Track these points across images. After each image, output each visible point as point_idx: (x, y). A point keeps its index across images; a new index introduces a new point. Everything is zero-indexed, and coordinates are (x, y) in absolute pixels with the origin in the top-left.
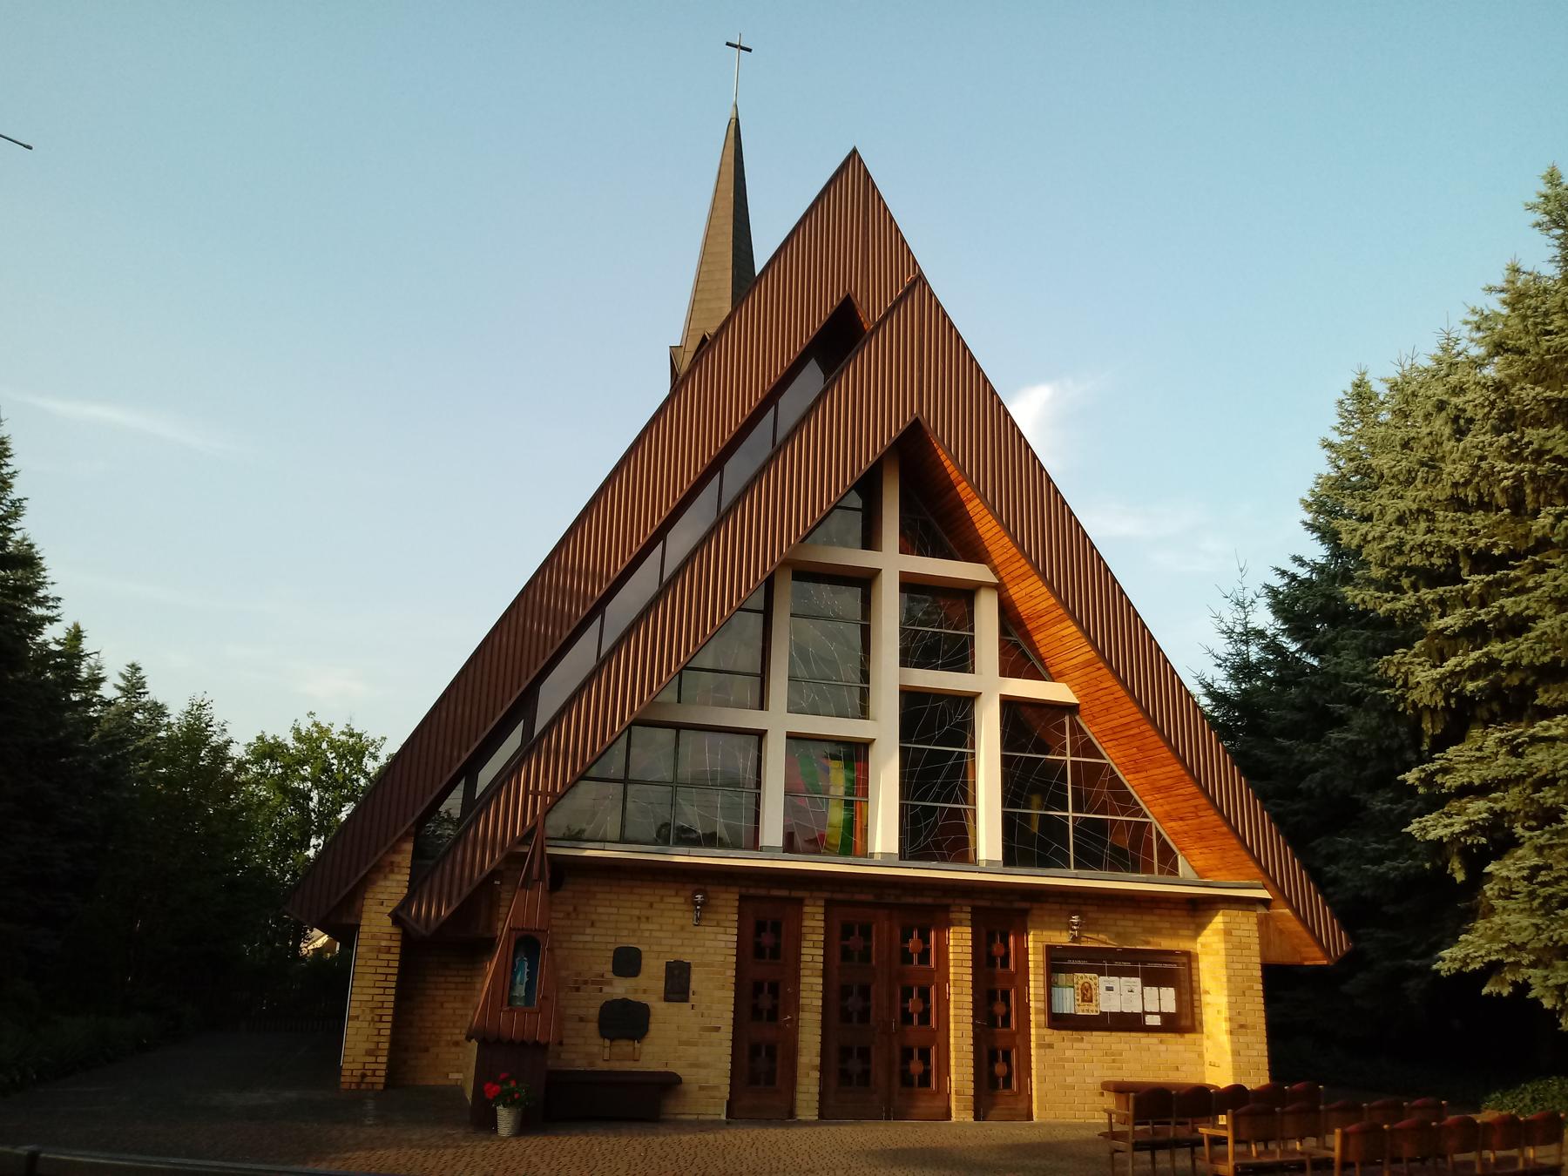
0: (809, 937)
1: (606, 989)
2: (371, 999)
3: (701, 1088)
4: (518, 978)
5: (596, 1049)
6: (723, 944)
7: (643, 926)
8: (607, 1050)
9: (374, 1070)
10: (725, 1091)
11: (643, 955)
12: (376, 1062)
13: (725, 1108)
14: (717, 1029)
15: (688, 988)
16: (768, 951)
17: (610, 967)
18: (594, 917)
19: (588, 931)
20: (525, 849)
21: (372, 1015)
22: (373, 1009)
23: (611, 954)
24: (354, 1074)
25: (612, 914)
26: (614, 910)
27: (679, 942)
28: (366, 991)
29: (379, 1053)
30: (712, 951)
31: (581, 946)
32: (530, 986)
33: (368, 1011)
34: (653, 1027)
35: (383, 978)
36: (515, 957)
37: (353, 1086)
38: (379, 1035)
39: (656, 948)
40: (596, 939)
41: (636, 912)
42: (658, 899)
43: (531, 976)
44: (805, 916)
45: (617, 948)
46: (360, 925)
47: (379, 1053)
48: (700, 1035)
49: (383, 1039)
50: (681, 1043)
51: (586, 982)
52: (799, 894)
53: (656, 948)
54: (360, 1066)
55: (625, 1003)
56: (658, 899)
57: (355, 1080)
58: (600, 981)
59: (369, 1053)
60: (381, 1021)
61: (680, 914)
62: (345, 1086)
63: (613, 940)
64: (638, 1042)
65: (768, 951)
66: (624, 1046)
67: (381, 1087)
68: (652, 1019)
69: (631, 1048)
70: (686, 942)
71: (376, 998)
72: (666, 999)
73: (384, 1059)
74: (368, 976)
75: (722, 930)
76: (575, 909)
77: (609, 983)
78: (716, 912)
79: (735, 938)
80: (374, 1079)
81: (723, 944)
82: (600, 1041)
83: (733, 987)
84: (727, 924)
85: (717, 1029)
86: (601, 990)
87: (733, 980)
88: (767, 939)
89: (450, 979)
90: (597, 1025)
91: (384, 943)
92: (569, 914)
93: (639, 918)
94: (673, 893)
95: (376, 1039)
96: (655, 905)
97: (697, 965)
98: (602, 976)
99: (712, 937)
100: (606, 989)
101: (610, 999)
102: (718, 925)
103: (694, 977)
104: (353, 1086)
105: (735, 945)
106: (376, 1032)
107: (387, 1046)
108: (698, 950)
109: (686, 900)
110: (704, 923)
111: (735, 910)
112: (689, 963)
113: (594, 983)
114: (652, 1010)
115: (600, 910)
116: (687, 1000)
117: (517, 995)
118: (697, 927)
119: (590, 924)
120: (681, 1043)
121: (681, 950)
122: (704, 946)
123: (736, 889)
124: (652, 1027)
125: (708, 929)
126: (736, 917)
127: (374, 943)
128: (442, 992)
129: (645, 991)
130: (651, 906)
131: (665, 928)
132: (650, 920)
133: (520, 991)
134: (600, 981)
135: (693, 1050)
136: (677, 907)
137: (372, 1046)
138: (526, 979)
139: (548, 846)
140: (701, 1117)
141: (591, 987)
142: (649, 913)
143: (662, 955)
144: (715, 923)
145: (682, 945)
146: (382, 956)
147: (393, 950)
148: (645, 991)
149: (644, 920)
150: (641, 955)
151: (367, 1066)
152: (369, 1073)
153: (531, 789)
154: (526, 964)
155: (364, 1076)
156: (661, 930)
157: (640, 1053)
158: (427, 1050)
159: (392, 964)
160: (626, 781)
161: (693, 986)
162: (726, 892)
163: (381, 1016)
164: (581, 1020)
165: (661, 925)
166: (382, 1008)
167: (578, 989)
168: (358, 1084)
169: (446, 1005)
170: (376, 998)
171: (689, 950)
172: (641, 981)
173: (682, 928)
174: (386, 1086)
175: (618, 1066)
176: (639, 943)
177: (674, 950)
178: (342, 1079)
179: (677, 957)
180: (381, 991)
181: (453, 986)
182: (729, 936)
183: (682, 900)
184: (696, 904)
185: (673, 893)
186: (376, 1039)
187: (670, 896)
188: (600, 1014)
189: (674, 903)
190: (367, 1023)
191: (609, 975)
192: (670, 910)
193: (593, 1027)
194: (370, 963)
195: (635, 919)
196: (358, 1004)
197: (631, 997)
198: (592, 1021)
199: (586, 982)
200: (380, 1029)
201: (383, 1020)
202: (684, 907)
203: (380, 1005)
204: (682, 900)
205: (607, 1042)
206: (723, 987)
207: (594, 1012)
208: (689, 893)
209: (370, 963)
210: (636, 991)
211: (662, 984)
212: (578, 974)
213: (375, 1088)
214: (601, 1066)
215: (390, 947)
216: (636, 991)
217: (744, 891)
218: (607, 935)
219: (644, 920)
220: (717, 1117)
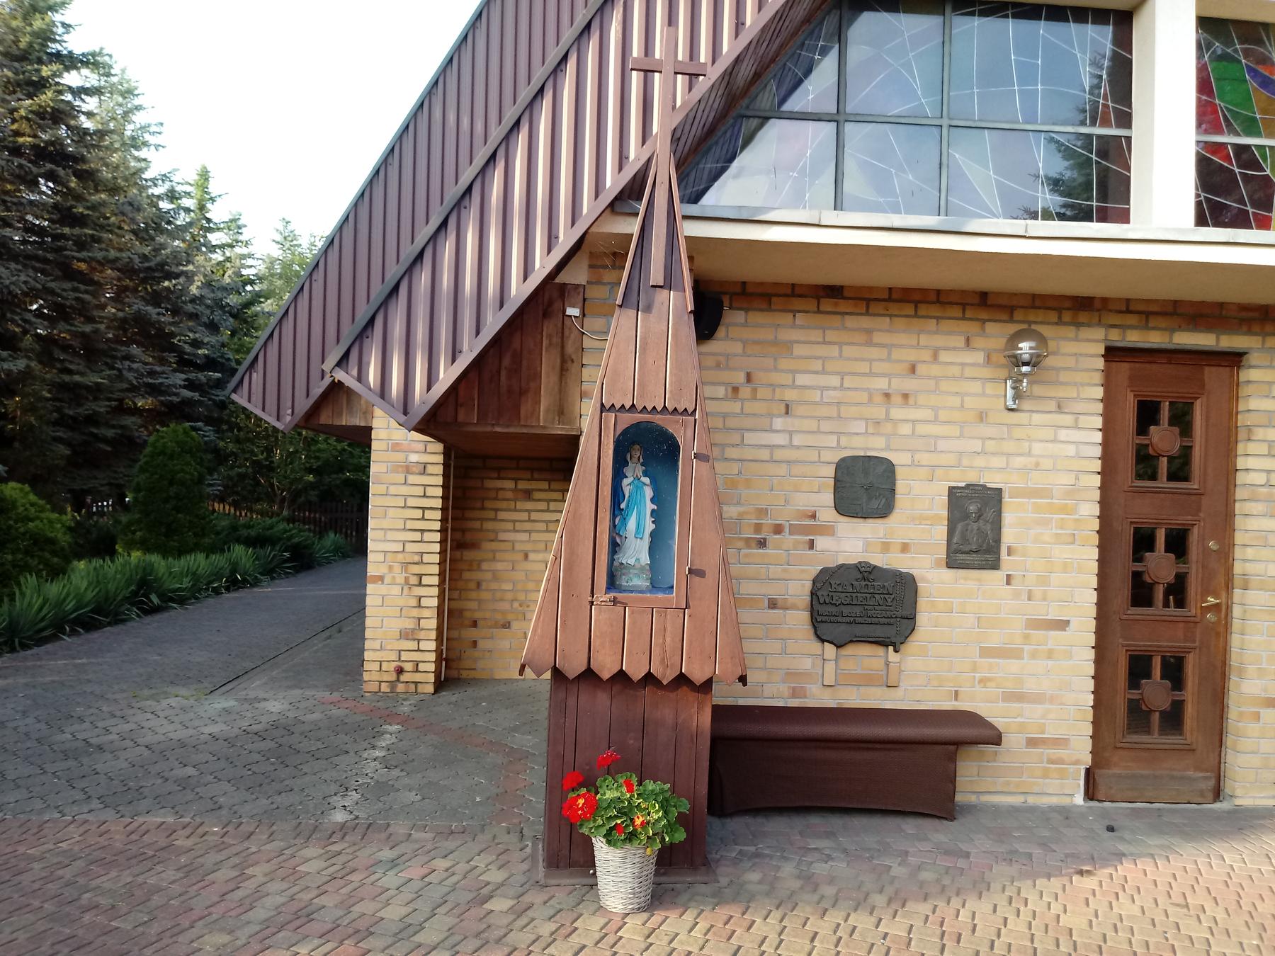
0: (1260, 433)
1: (822, 542)
2: (533, 514)
3: (1032, 743)
4: (632, 524)
5: (806, 664)
6: (1071, 450)
7: (897, 413)
8: (830, 667)
9: (417, 663)
10: (1082, 750)
11: (900, 473)
12: (419, 650)
13: (1082, 782)
14: (1063, 625)
15: (998, 541)
16: (1164, 462)
17: (828, 497)
18: (790, 395)
19: (779, 423)
20: (632, 227)
21: (404, 575)
22: (405, 565)
23: (830, 471)
24: (384, 668)
25: (828, 388)
26: (834, 381)
27: (976, 445)
28: (391, 536)
29: (422, 635)
30: (1046, 463)
31: (765, 455)
32: (658, 542)
33: (397, 568)
34: (924, 618)
35: (419, 514)
36: (618, 475)
37: (385, 688)
38: (419, 606)
39: (924, 458)
40: (797, 440)
41: (882, 384)
42: (927, 355)
43: (661, 516)
44: (1244, 391)
45: (843, 460)
46: (371, 428)
47: (422, 635)
48: (1027, 637)
49: (426, 613)
50: (986, 652)
51: (778, 529)
52: (1229, 342)
53: (924, 458)
54: (394, 656)
55: (866, 572)
56: (927, 355)
57: (386, 677)
58: (810, 528)
59: (405, 635)
60: (420, 584)
61: (976, 387)
62: (373, 687)
63: (832, 441)
64: (896, 651)
65: (1164, 462)
66: (865, 657)
67: (431, 689)
68: (922, 603)
69: (882, 661)
70: (990, 445)
71: (409, 547)
72: (951, 564)
73: (432, 646)
74: (391, 512)
75: (1067, 419)
76: (749, 378)
77: (828, 530)
78: (1057, 383)
79: (1098, 437)
80: (417, 677)
81: (1071, 450)
82: (816, 646)
83: (1095, 539)
84: (1079, 407)
85: (1063, 625)
86: (811, 545)
87: (1096, 525)
88: (1162, 437)
89: (534, 516)
90: (805, 616)
91: (414, 458)
92: (736, 390)
93: (887, 395)
94: (959, 341)
95: (416, 613)
96: (921, 369)
97: (1017, 493)
98: (814, 516)
99: (1047, 433)
100: (822, 542)
101: (831, 565)
102: (1060, 409)
103: (1009, 518)
104: (385, 688)
105: (1098, 451)
106: (414, 602)
107: (433, 623)
108: (1018, 462)
109: (988, 359)
110: (1026, 405)
111: (1098, 378)
112: (1000, 490)
113: (795, 530)
114: (921, 585)
115: (802, 379)
116: (995, 566)
117: (632, 562)
118: (1012, 414)
119: (783, 410)
120: (986, 652)
121: (980, 462)
122: (1029, 454)
123: (1099, 333)
124: (923, 618)
125: (1037, 418)
126: (1099, 392)
127: (399, 457)
128: (524, 536)
129: (905, 548)
130: (913, 369)
131: (943, 415)
132: (911, 401)
133: (636, 552)
134: (810, 528)
135: (1013, 666)
136: (969, 372)
137: (410, 624)
138: (650, 527)
139: (685, 217)
140: (1032, 800)
141: (788, 539)
142: (909, 384)
143: (939, 472)
144: (1052, 405)
145: (983, 452)
146: (412, 479)
147: (430, 469)
148: (905, 548)
149: (897, 399)
150: (893, 472)
151: (404, 656)
152: (408, 667)
153: (635, 54)
154: (649, 492)
155: (400, 671)
156: (936, 420)
157: (901, 671)
158: (507, 625)
159: (430, 492)
160: (838, 118)
161: (1009, 535)
162: (1076, 339)
163: (420, 576)
164: (773, 604)
165: (935, 409)
166: (421, 562)
167: (762, 543)
168: (393, 684)
169: (532, 556)
170: (409, 547)
171: (998, 462)
172: (896, 526)
173: (982, 417)
174: (440, 685)
175: (854, 698)
176: (888, 448)
177: (965, 462)
178: (366, 676)
179: (972, 478)
180: (417, 536)
181: (542, 526)
182: (1083, 433)
183: (979, 357)
184: (1017, 362)
185: (959, 341)
186: (416, 613)
187: (954, 349)
188: (813, 594)
189: (963, 365)
190: (399, 588)
191: (828, 514)
192: (954, 378)
193: (799, 619)
194: (393, 490)
195: (878, 398)
196: (380, 557)
197: (878, 560)
198: (797, 608)
199: (778, 529)
200: (420, 598)
201: (424, 582)
202: (986, 372)
203: (417, 558)
204: (979, 357)
205: (830, 649)
206: (1073, 540)
207: (800, 590)
208: (1000, 342)
209: (393, 490)
210: (886, 547)
211: (941, 532)
212: (762, 512)
213: (420, 690)
214: (819, 698)
215: (425, 465)
216: (886, 547)
217: (1116, 337)
218: (818, 432)
219: (897, 399)
220: (1065, 801)
